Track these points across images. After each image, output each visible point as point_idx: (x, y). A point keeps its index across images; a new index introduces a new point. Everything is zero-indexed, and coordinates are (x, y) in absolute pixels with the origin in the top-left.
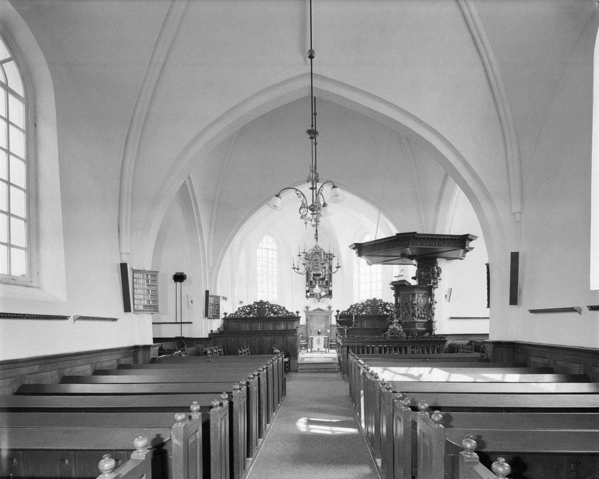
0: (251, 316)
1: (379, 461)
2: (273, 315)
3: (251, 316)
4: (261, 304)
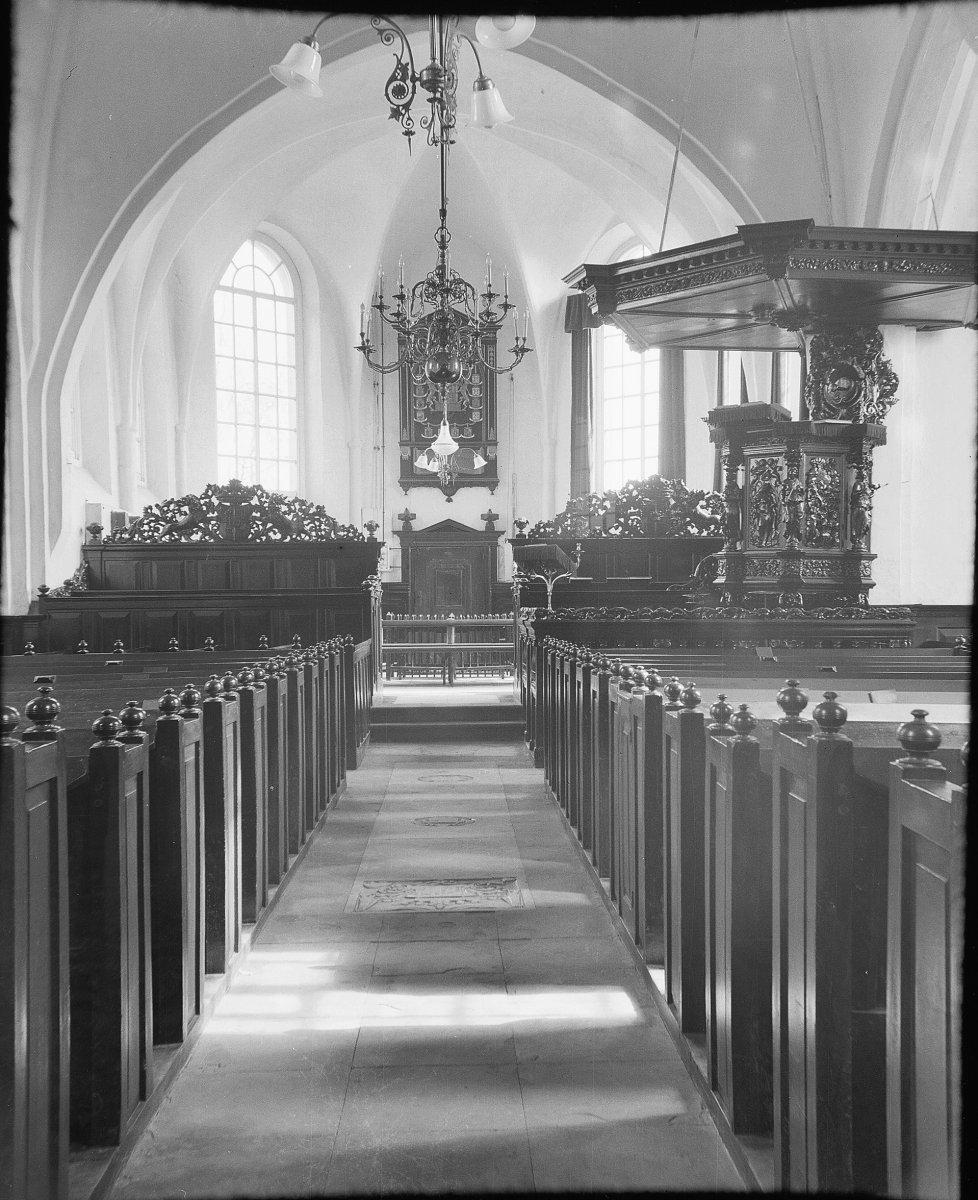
0: (196, 537)
1: (658, 976)
2: (278, 536)
3: (196, 537)
4: (235, 494)
